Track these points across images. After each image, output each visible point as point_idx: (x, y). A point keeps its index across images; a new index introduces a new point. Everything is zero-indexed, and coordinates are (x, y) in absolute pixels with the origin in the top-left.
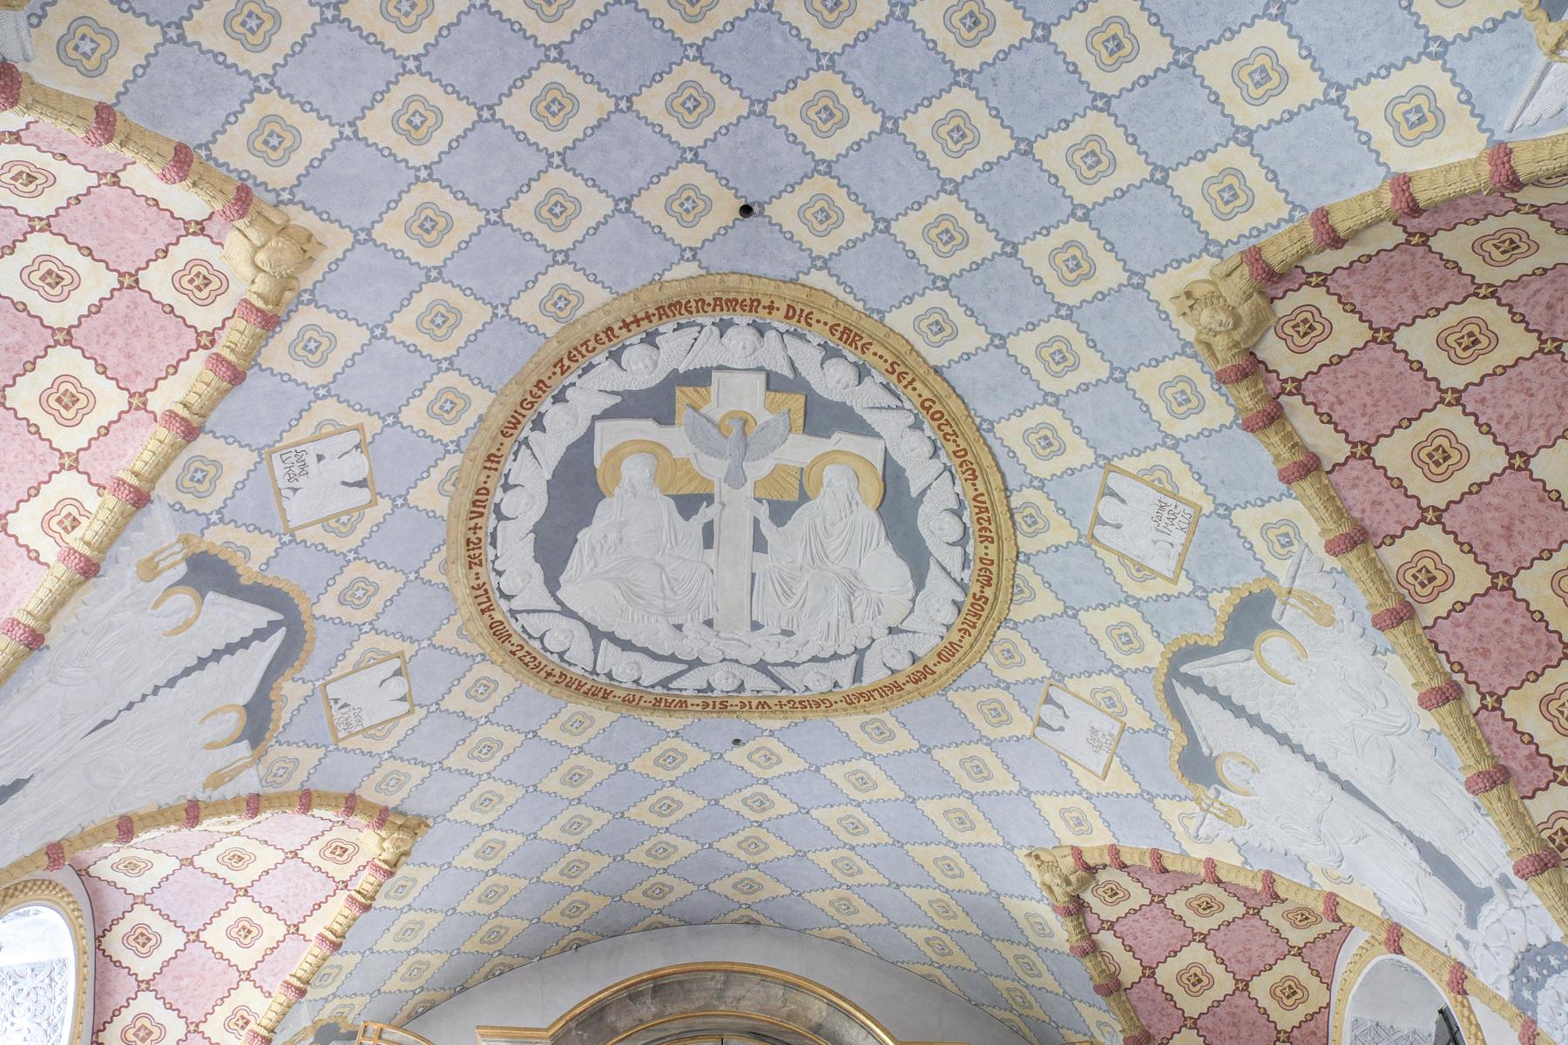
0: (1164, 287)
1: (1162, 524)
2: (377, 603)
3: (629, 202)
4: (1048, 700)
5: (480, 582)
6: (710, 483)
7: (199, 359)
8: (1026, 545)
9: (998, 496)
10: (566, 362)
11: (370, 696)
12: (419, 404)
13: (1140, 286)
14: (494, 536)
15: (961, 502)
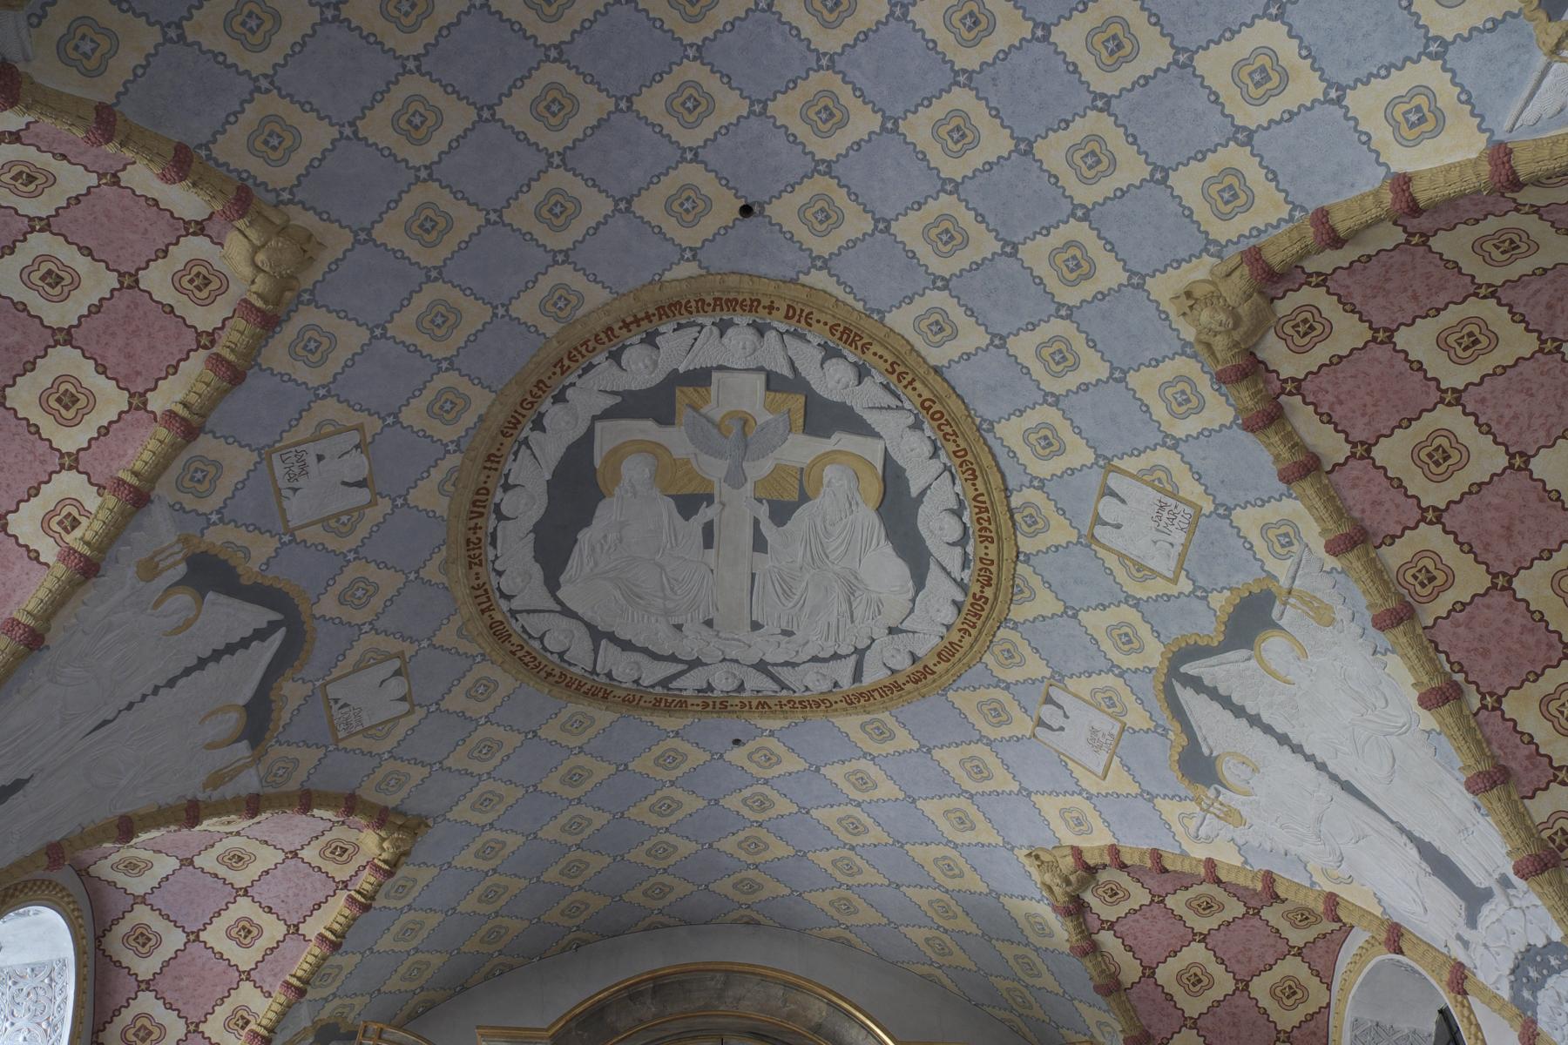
0: (1164, 287)
1: (1162, 524)
2: (377, 603)
3: (629, 202)
4: (1049, 700)
5: (480, 582)
6: (710, 483)
7: (197, 361)
8: (1026, 545)
10: (566, 362)
11: (371, 696)
12: (420, 404)
13: (1140, 286)
14: (494, 536)
15: (961, 502)
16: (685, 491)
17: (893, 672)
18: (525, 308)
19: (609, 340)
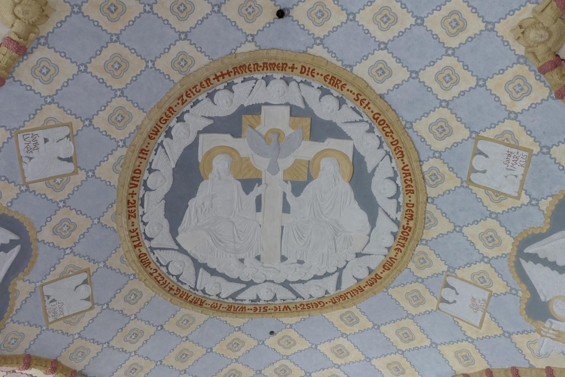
0: (504, 28)
1: (510, 165)
2: (75, 235)
3: (220, 7)
4: (447, 285)
5: (134, 228)
6: (260, 172)
8: (432, 192)
9: (415, 164)
10: (185, 97)
11: (69, 296)
12: (104, 115)
13: (492, 30)
14: (142, 199)
15: (395, 172)
16: (247, 177)
17: (359, 280)
18: (163, 64)
19: (206, 85)
